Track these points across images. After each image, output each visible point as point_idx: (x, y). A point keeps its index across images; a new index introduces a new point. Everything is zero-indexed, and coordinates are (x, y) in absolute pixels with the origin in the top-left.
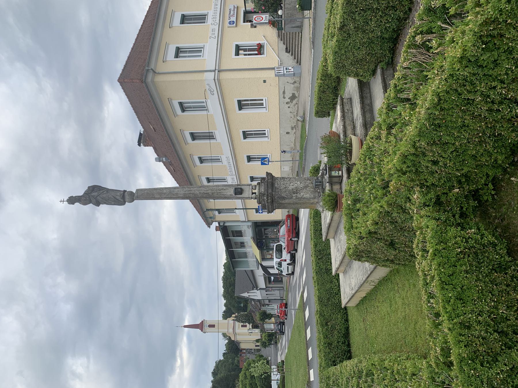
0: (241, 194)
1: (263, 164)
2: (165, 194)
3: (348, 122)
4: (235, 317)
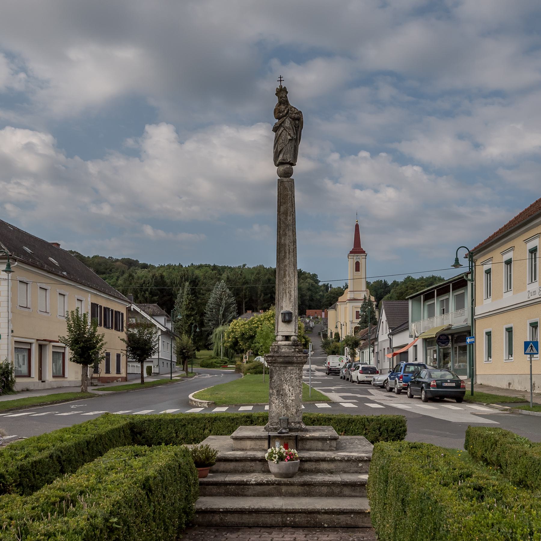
0: (282, 321)
1: (526, 344)
2: (286, 219)
3: (342, 465)
4: (369, 300)
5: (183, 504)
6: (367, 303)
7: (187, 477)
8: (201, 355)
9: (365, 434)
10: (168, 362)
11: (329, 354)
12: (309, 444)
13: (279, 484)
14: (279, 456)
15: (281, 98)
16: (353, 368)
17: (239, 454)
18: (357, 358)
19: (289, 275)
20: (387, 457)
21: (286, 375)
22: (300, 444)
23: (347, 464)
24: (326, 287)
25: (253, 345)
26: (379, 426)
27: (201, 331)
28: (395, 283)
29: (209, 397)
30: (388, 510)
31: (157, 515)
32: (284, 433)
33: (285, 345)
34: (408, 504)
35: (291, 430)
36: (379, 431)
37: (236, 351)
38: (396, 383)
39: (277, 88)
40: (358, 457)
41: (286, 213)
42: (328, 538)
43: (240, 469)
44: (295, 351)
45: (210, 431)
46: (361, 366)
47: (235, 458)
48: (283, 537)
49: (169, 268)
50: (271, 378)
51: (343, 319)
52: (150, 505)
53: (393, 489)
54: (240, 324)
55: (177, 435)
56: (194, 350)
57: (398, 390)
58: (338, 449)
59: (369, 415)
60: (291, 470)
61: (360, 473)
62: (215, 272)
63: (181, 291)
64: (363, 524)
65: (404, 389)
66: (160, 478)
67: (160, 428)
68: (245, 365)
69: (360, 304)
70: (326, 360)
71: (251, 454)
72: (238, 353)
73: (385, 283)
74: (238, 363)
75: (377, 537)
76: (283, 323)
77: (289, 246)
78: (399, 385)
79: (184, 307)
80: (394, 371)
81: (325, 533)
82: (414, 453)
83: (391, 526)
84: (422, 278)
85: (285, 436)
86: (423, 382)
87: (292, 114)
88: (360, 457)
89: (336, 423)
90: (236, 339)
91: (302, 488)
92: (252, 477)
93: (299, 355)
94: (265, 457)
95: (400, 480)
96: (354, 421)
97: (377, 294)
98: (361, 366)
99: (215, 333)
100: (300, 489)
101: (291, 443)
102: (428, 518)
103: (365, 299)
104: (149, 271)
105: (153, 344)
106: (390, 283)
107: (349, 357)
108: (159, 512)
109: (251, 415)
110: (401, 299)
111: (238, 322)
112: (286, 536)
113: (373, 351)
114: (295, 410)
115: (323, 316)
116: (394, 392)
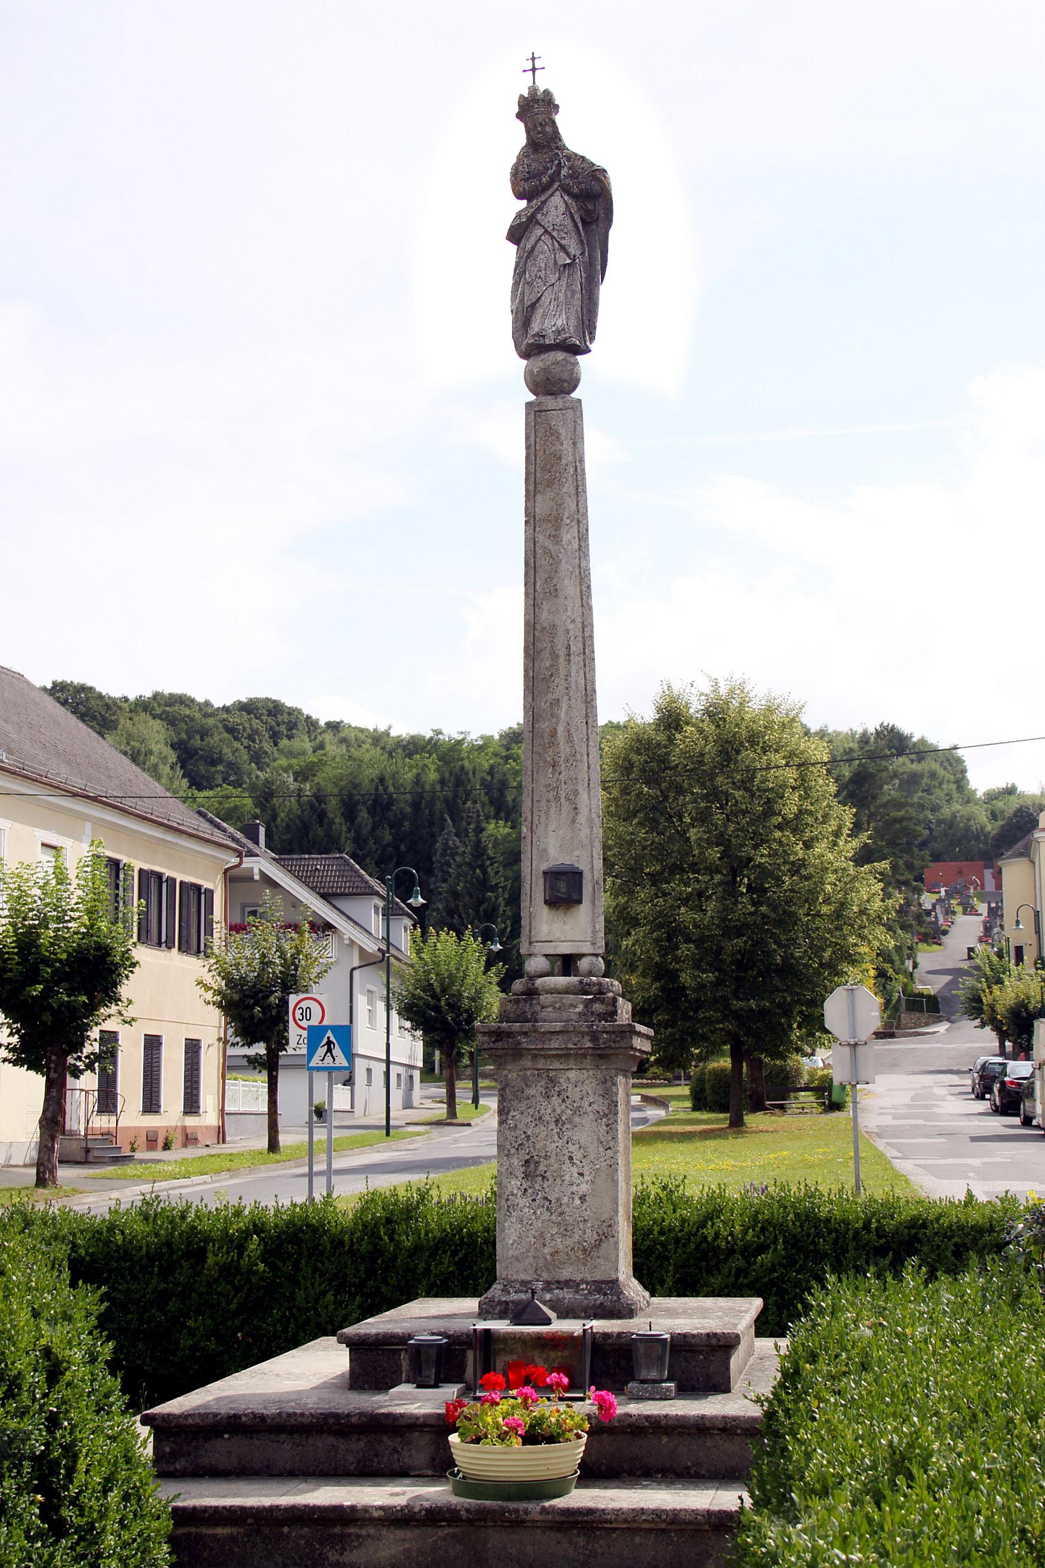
0: (546, 902)
10: (373, 1065)
39: (521, 96)
41: (555, 521)
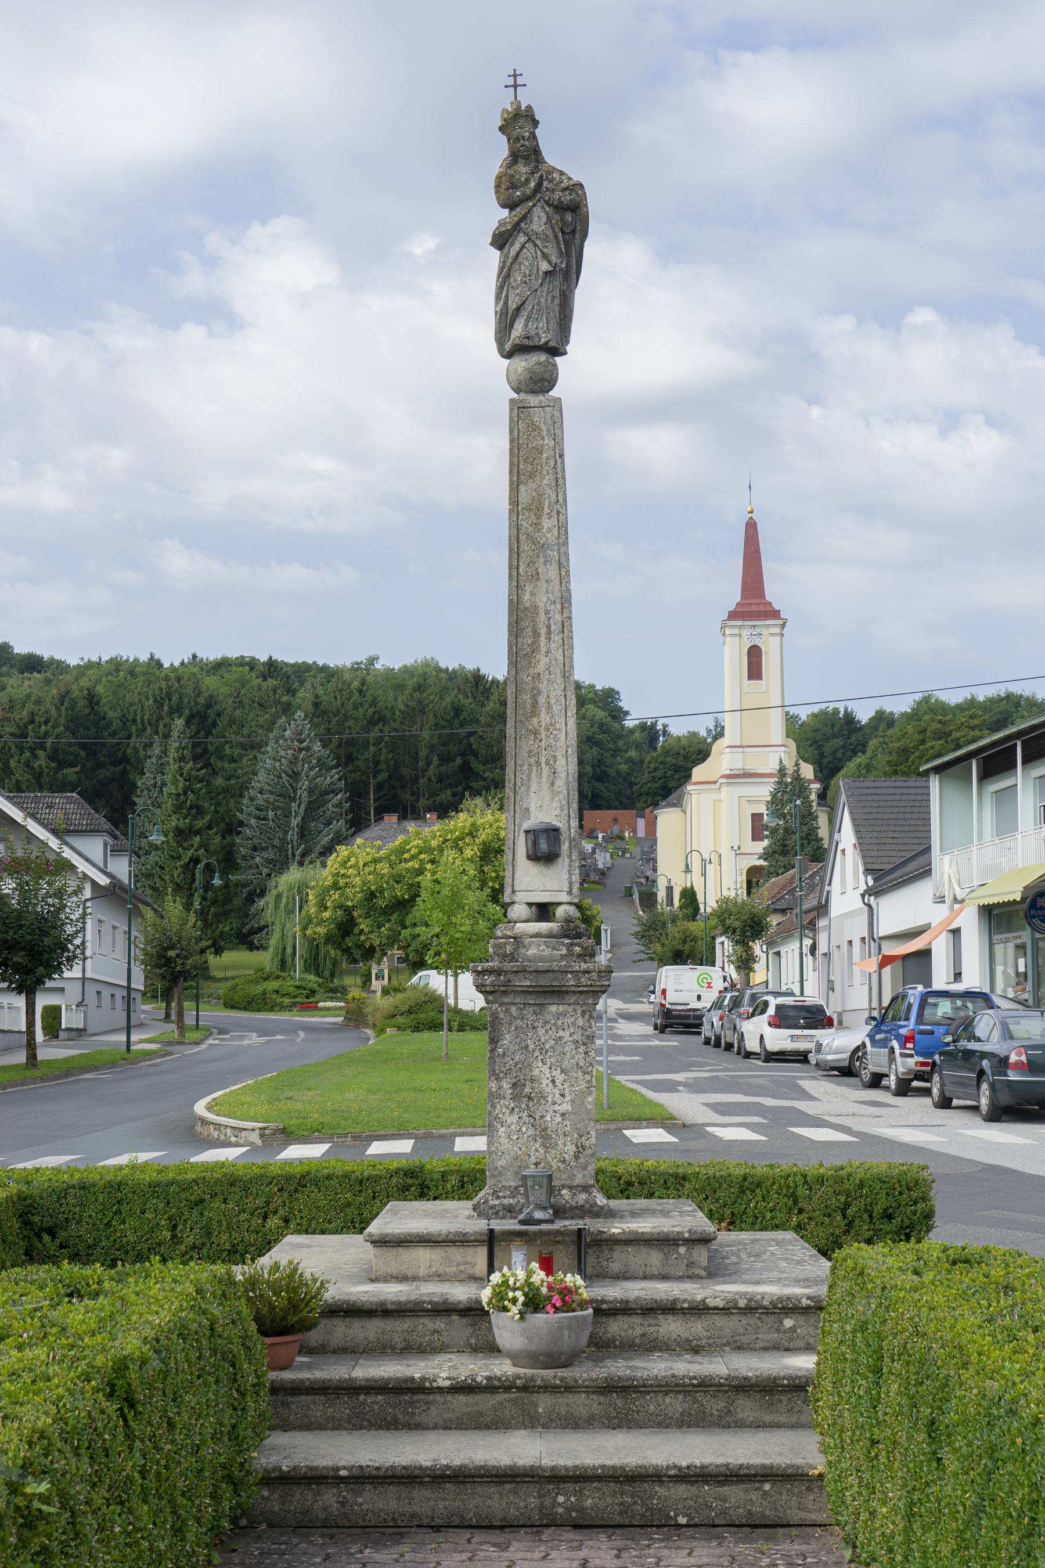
0: (529, 857)
2: (537, 526)
4: (797, 777)
5: (216, 1453)
6: (787, 790)
7: (233, 1365)
8: (226, 968)
9: (799, 1228)
11: (663, 962)
12: (618, 1260)
13: (528, 1388)
14: (526, 1295)
15: (517, 139)
16: (746, 1008)
17: (393, 1292)
18: (759, 975)
19: (549, 707)
20: (879, 1292)
21: (541, 1032)
22: (591, 1260)
23: (745, 1321)
24: (650, 732)
25: (405, 933)
26: (843, 1198)
27: (226, 886)
28: (882, 719)
29: (262, 1110)
30: (883, 1459)
31: (151, 1483)
32: (539, 1222)
33: (537, 935)
34: (949, 1436)
35: (559, 1212)
36: (844, 1217)
37: (347, 951)
38: (892, 1059)
39: (505, 110)
40: (780, 1299)
42: (692, 1561)
43: (397, 1339)
44: (570, 954)
45: (286, 1221)
46: (773, 1002)
47: (383, 1304)
48: (544, 1558)
49: (118, 670)
50: (494, 1041)
51: (706, 842)
52: (131, 1448)
53: (899, 1393)
54: (364, 857)
55: (174, 1236)
56: (203, 951)
57: (899, 1081)
58: (714, 1272)
59: (810, 1164)
60: (567, 1341)
61: (787, 1350)
62: (271, 682)
63: (157, 750)
64: (803, 1515)
65: (919, 1076)
66: (156, 1364)
67: (118, 1212)
68: (379, 1001)
69: (764, 791)
70: (653, 981)
71: (431, 1291)
72: (355, 961)
73: (849, 719)
74: (355, 993)
75: (848, 1554)
76: (530, 864)
77: (547, 612)
78: (904, 1064)
79: (169, 804)
80: (884, 1017)
81: (682, 1543)
82: (963, 1278)
83: (894, 1509)
84: (972, 703)
85: (541, 1233)
86: (984, 1055)
87: (553, 191)
88: (789, 1299)
89: (702, 1189)
90: (348, 911)
91: (602, 1399)
92: (440, 1366)
93: (584, 966)
94: (480, 1303)
95: (922, 1362)
96: (759, 1185)
97: (822, 755)
98: (773, 1002)
99: (274, 892)
100: (594, 1404)
101: (562, 1256)
102: (1011, 1474)
103: (782, 772)
104: (48, 682)
105: (69, 929)
106: (864, 715)
107: (732, 971)
108: (158, 1474)
109: (422, 1167)
110: (904, 774)
111: (353, 854)
112: (553, 1554)
113: (813, 949)
114: (571, 1148)
115: (641, 833)
116: (887, 1088)
